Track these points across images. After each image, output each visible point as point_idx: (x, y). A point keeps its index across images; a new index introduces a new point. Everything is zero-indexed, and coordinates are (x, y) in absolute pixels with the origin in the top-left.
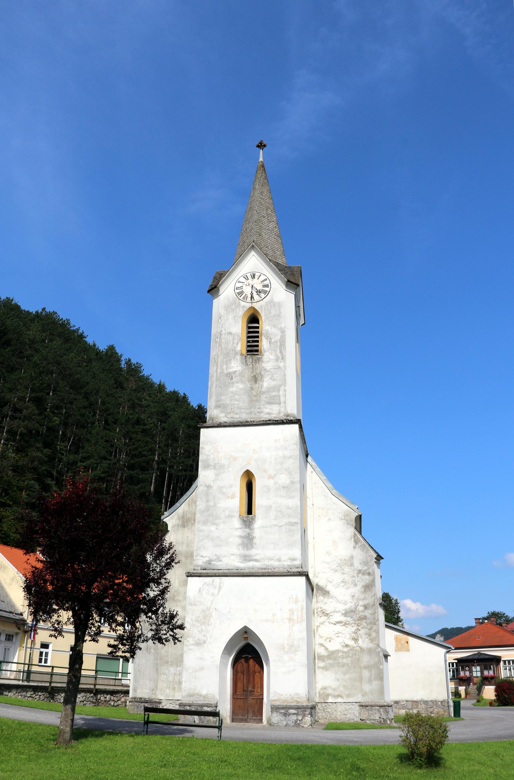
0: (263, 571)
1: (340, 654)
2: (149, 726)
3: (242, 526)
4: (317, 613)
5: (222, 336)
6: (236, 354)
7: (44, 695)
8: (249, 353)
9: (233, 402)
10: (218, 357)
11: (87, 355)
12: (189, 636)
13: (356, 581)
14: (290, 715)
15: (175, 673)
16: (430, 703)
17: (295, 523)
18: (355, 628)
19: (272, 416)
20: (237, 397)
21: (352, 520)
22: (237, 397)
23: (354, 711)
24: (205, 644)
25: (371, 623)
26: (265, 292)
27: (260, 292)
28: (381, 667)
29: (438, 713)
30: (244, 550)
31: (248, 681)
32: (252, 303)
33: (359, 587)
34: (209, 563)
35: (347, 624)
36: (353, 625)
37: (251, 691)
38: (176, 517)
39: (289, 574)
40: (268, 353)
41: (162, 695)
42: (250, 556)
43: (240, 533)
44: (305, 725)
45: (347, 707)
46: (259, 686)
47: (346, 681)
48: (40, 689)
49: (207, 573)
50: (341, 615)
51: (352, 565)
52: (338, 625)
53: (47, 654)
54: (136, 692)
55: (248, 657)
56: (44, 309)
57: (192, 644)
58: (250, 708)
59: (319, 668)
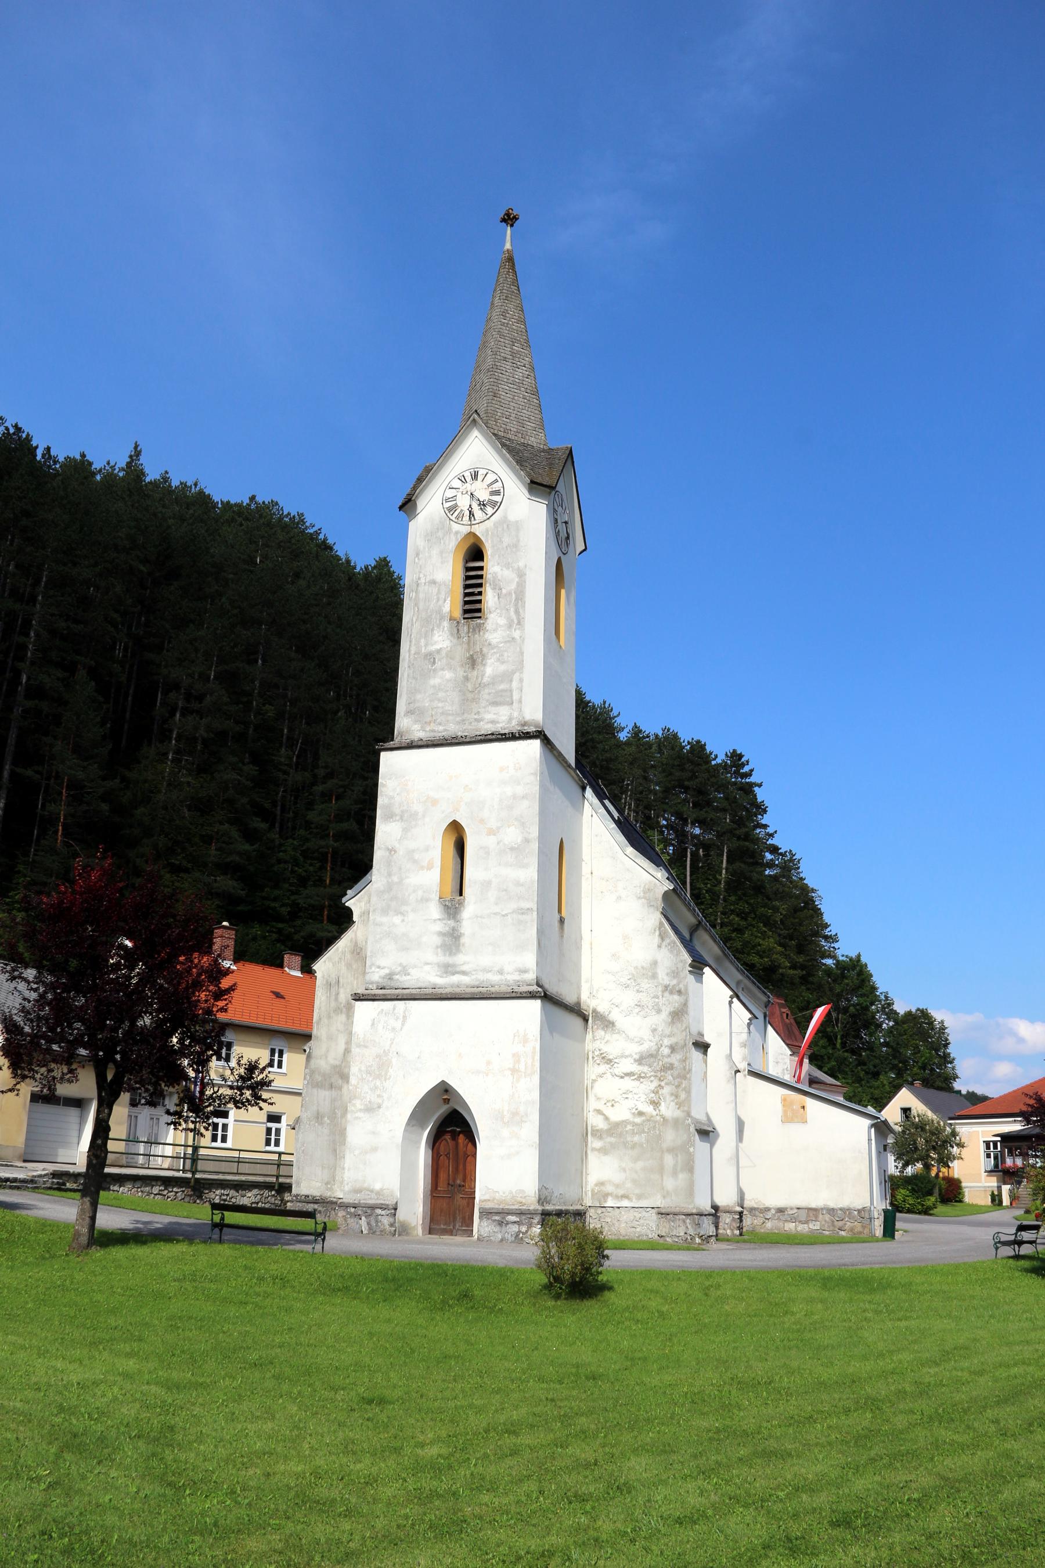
0: (475, 990)
1: (629, 1127)
2: (223, 1232)
4: (593, 1058)
5: (419, 588)
6: (442, 618)
7: (183, 1191)
8: (466, 616)
9: (436, 704)
10: (412, 625)
11: (328, 583)
12: (355, 1097)
13: (660, 1004)
16: (839, 1212)
18: (656, 1083)
19: (498, 725)
20: (441, 694)
22: (441, 694)
25: (679, 1076)
26: (493, 504)
27: (484, 505)
28: (691, 1149)
29: (852, 1230)
31: (456, 1170)
32: (471, 525)
33: (664, 1015)
36: (652, 1078)
37: (460, 1186)
39: (514, 995)
40: (495, 614)
42: (454, 966)
43: (439, 927)
45: (638, 1215)
47: (636, 1172)
48: (177, 1182)
49: (384, 995)
50: (632, 1061)
51: (654, 976)
52: (626, 1078)
53: (278, 1131)
54: (300, 1187)
55: (455, 1131)
56: (253, 498)
57: (360, 1110)
59: (593, 1149)
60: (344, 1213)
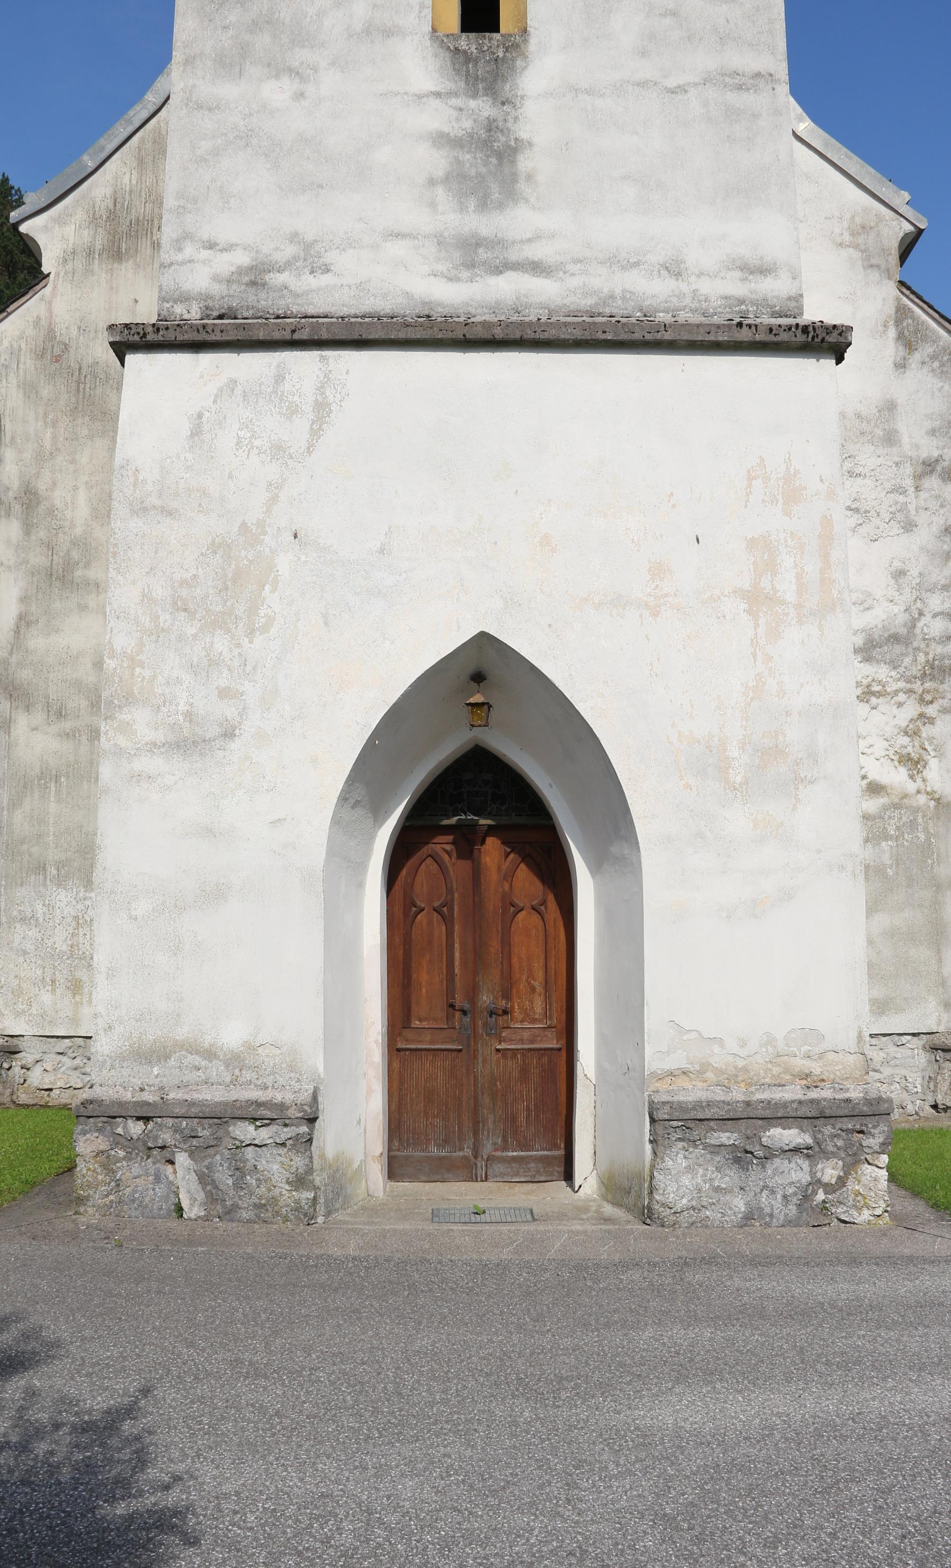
3: (450, 86)
12: (129, 699)
13: (912, 508)
14: (770, 1154)
15: (76, 918)
17: (758, 75)
18: (911, 709)
21: (884, 251)
23: (904, 1072)
24: (235, 745)
30: (462, 208)
34: (253, 283)
35: (873, 694)
36: (902, 697)
38: (80, 215)
39: (745, 335)
41: (18, 1014)
44: (859, 1210)
46: (536, 984)
51: (890, 439)
55: (475, 825)
57: (153, 747)
58: (486, 1100)
60: (102, 1143)
